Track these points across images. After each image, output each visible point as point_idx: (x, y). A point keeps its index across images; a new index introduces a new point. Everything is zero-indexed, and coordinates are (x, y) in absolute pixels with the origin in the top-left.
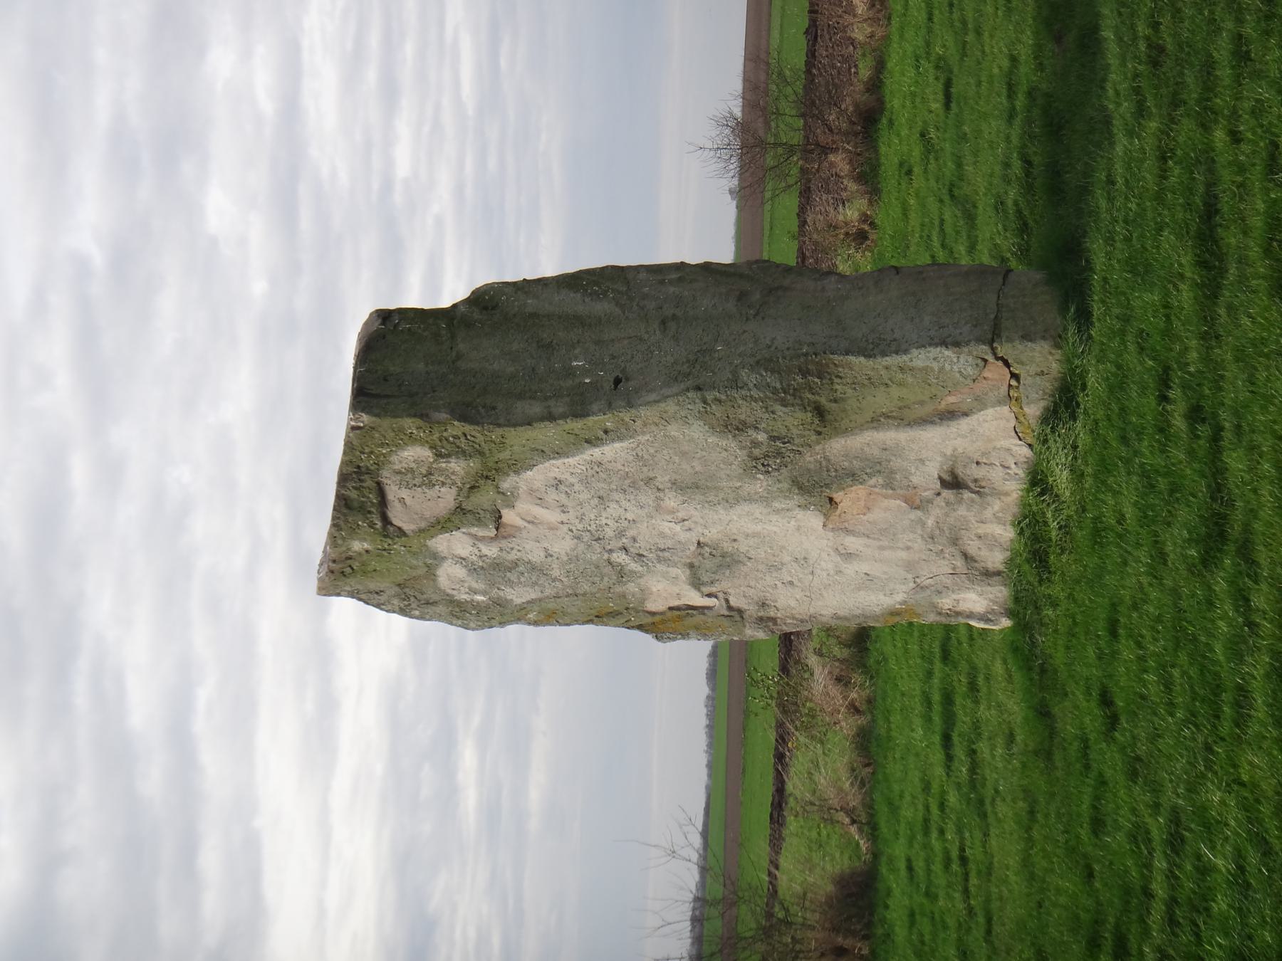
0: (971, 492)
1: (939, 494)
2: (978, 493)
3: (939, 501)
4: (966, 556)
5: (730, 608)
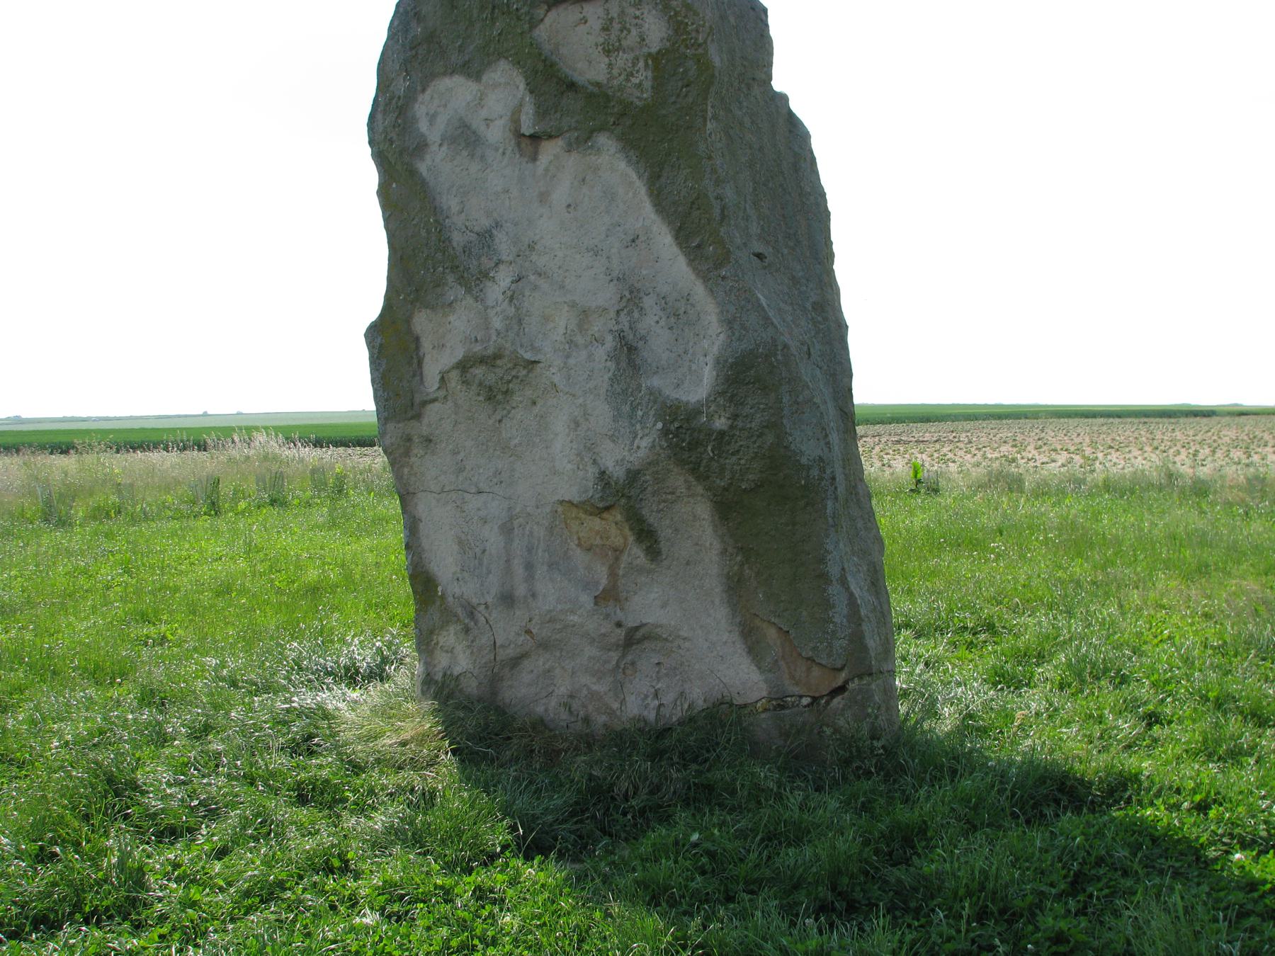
0: (618, 661)
1: (656, 695)
2: (617, 665)
3: (606, 627)
4: (523, 656)
5: (424, 403)
